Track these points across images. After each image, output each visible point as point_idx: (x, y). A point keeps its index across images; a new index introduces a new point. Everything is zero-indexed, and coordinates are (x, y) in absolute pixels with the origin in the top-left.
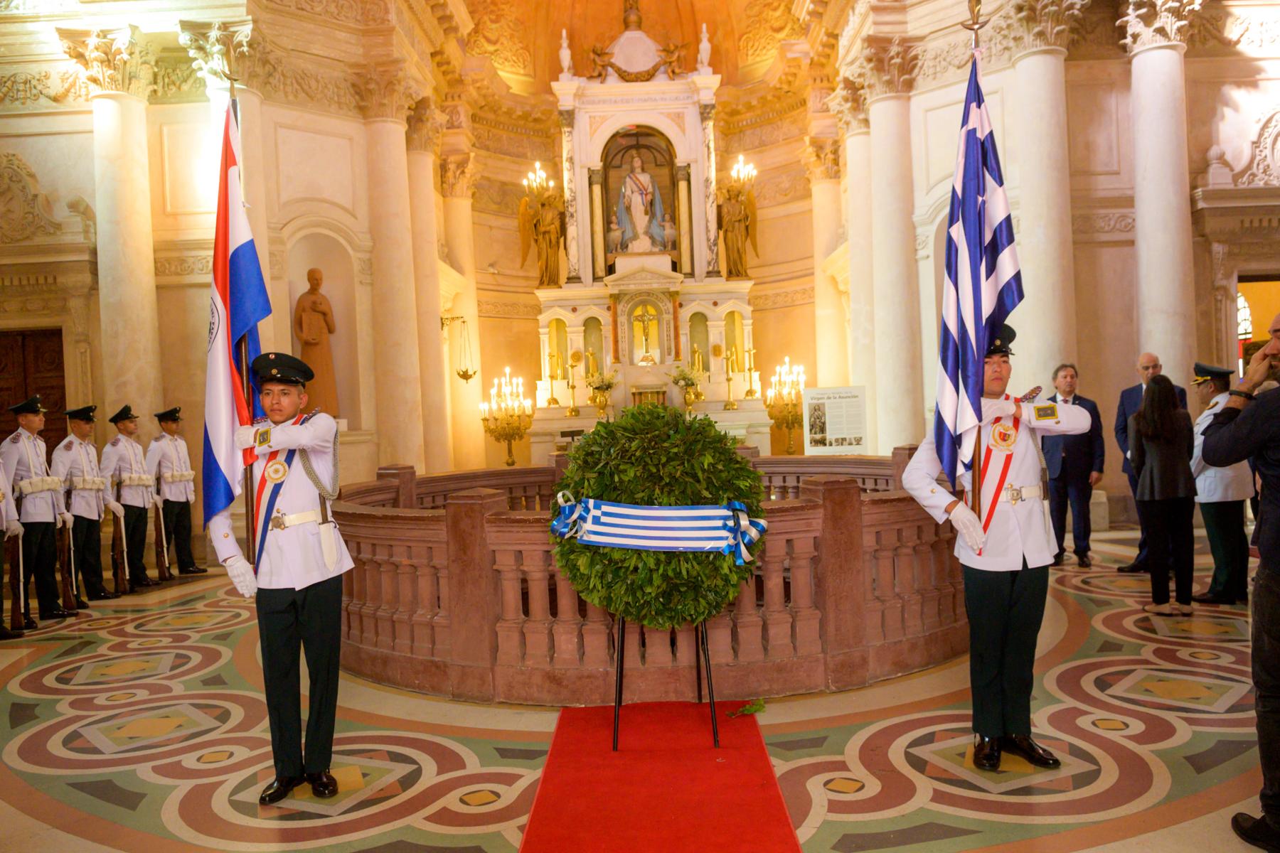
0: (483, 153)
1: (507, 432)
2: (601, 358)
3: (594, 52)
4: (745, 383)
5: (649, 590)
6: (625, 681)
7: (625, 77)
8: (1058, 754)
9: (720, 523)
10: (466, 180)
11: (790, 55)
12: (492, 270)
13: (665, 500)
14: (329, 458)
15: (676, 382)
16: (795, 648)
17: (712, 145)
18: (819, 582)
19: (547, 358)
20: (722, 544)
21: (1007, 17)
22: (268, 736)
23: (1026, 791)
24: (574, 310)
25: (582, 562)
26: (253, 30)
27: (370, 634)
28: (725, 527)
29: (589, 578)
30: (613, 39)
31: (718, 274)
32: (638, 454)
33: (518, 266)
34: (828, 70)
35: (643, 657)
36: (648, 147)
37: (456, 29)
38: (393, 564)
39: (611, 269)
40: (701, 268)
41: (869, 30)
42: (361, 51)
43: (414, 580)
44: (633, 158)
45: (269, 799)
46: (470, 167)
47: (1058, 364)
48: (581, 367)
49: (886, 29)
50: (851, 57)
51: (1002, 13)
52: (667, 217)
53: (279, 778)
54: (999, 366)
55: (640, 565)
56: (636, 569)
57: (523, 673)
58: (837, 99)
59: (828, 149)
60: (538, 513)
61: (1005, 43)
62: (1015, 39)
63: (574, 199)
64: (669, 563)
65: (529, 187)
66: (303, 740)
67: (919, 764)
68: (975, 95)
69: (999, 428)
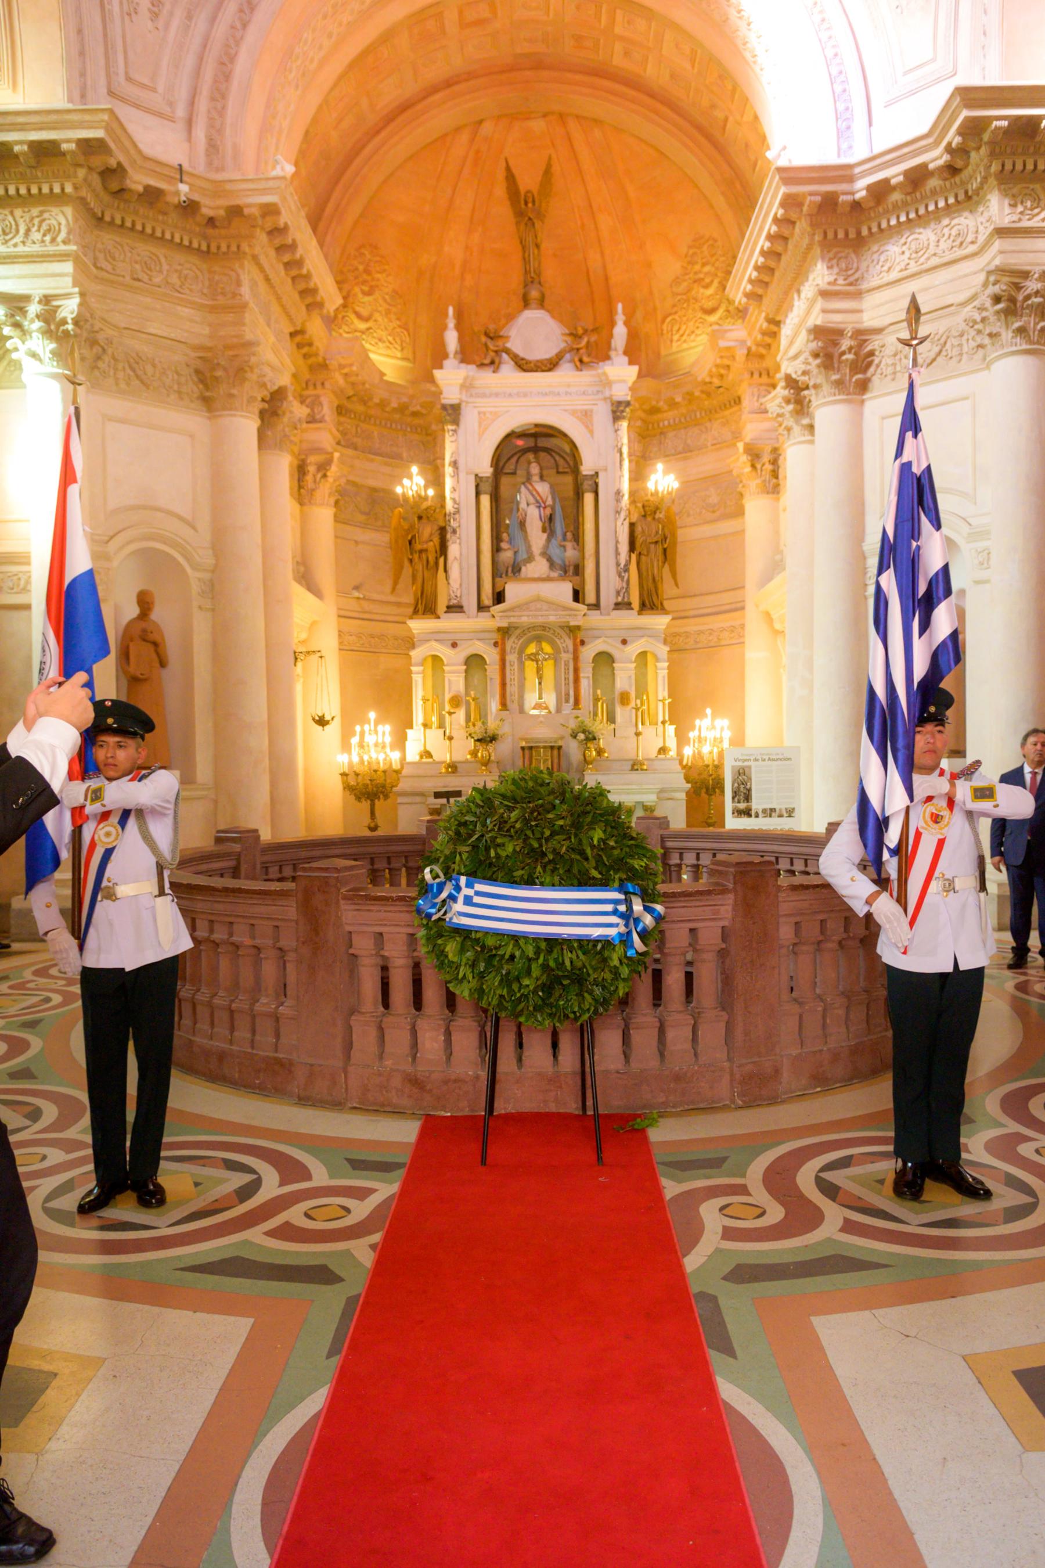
0: (350, 452)
1: (370, 790)
2: (485, 705)
3: (486, 334)
4: (657, 738)
5: (526, 982)
6: (497, 1087)
7: (523, 365)
8: (990, 1184)
9: (609, 908)
10: (328, 485)
11: (722, 344)
12: (356, 594)
13: (548, 879)
14: (169, 821)
15: (574, 736)
16: (696, 1055)
17: (625, 450)
18: (727, 980)
19: (421, 702)
20: (612, 932)
21: (981, 309)
22: (88, 1139)
23: (951, 1223)
24: (454, 645)
25: (451, 948)
26: (80, 305)
27: (203, 1026)
28: (615, 912)
29: (458, 968)
30: (511, 318)
31: (628, 606)
32: (518, 825)
33: (388, 588)
34: (768, 363)
35: (520, 1060)
36: (547, 450)
37: (320, 305)
38: (233, 944)
39: (499, 597)
40: (608, 597)
41: (816, 319)
42: (207, 331)
43: (257, 963)
44: (529, 463)
45: (86, 1209)
46: (334, 470)
47: (1031, 727)
48: (461, 714)
49: (837, 318)
50: (794, 351)
51: (976, 303)
52: (569, 535)
53: (100, 1183)
54: (933, 736)
55: (517, 954)
56: (512, 957)
57: (380, 1075)
58: (776, 399)
59: (766, 458)
60: (404, 890)
61: (979, 340)
62: (990, 335)
63: (458, 511)
64: (550, 951)
65: (404, 494)
66: (128, 1144)
67: (830, 1191)
68: (911, 423)
69: (931, 808)
